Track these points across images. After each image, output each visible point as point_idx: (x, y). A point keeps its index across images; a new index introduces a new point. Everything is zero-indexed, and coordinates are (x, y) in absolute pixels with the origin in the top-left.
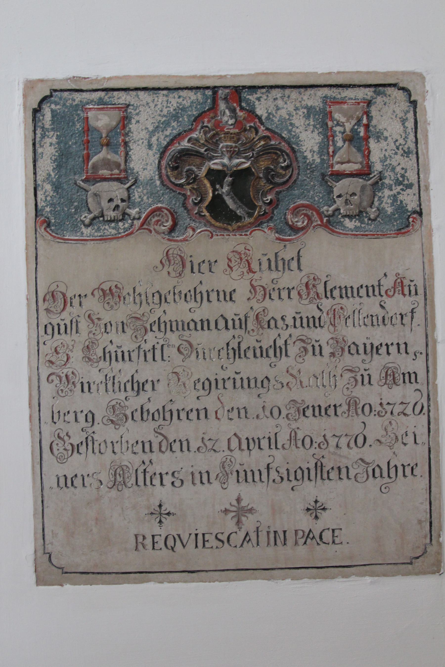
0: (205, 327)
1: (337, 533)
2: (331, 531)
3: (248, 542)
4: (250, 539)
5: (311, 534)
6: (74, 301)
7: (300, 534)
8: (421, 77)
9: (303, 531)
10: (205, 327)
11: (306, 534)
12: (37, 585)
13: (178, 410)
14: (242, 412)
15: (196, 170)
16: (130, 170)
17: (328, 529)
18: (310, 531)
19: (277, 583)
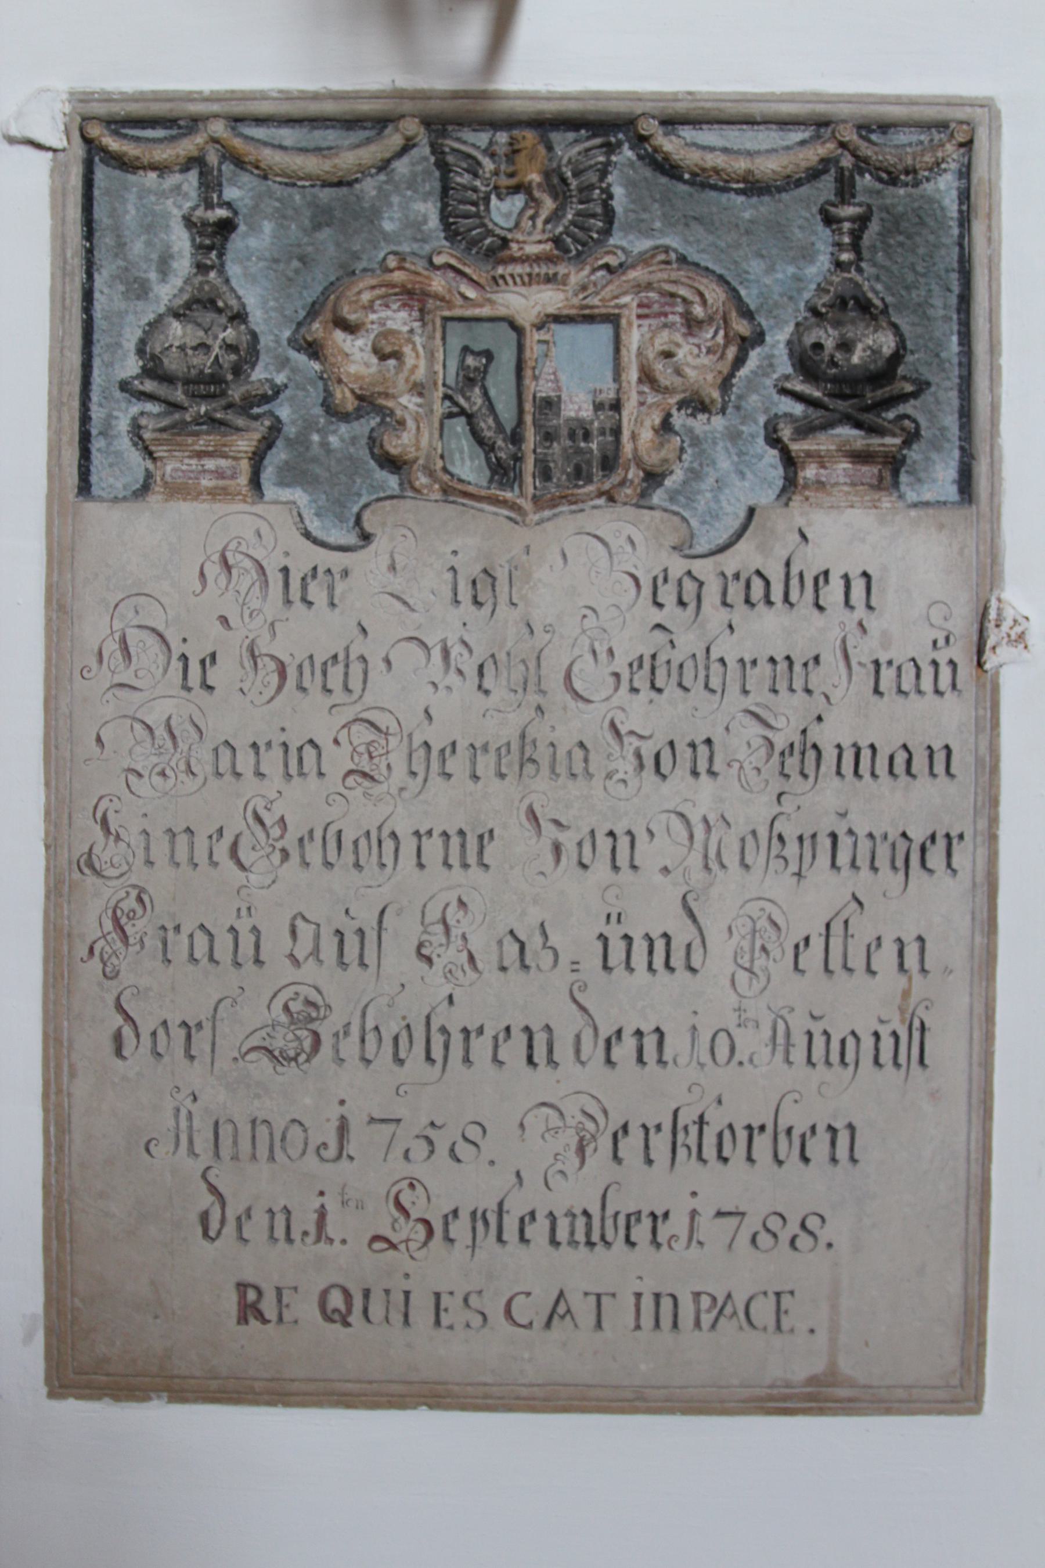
0: (939, 768)
1: (786, 1300)
2: (772, 1298)
3: (562, 1317)
4: (569, 1311)
5: (729, 1304)
6: (330, 670)
7: (705, 1302)
8: (987, 105)
9: (714, 1299)
10: (939, 768)
11: (720, 1303)
12: (52, 1395)
13: (466, 1031)
14: (650, 1043)
15: (536, 270)
16: (411, 197)
17: (765, 1293)
18: (729, 1296)
19: (28, 1338)
